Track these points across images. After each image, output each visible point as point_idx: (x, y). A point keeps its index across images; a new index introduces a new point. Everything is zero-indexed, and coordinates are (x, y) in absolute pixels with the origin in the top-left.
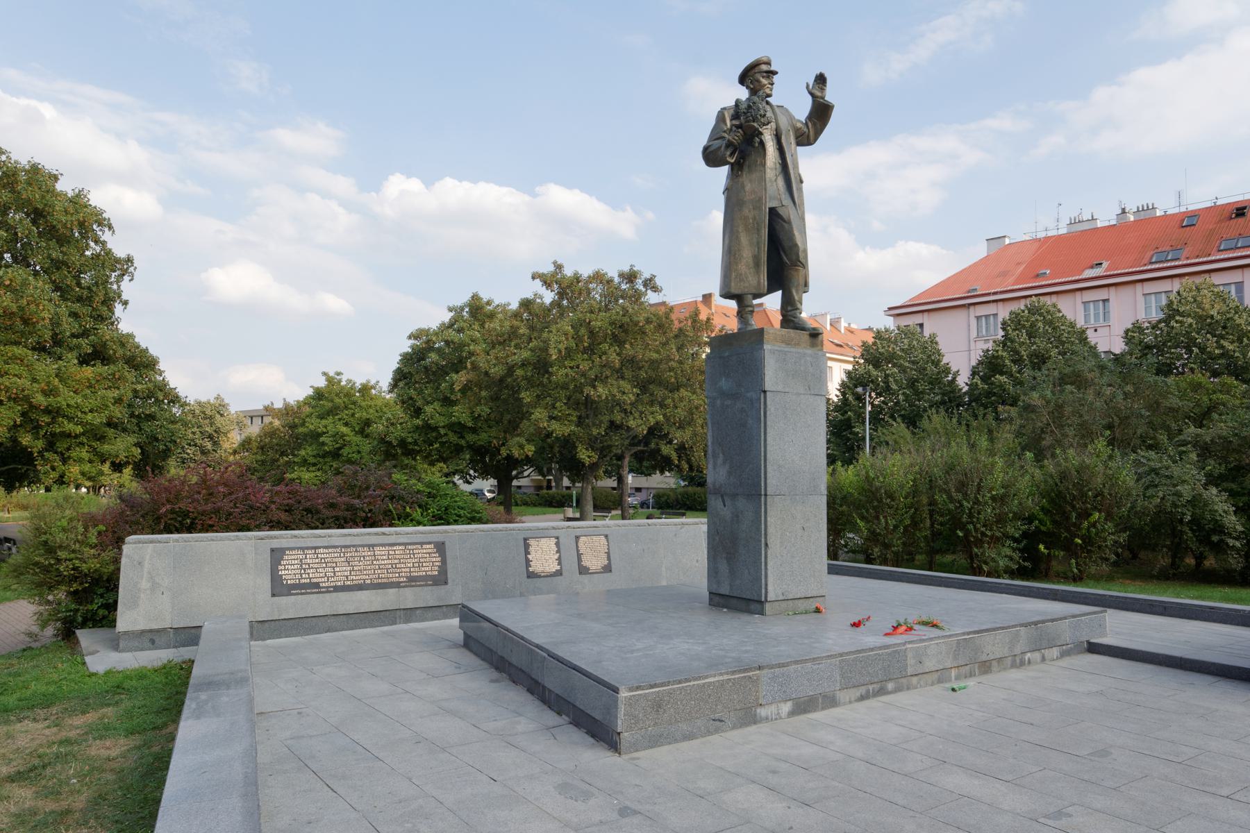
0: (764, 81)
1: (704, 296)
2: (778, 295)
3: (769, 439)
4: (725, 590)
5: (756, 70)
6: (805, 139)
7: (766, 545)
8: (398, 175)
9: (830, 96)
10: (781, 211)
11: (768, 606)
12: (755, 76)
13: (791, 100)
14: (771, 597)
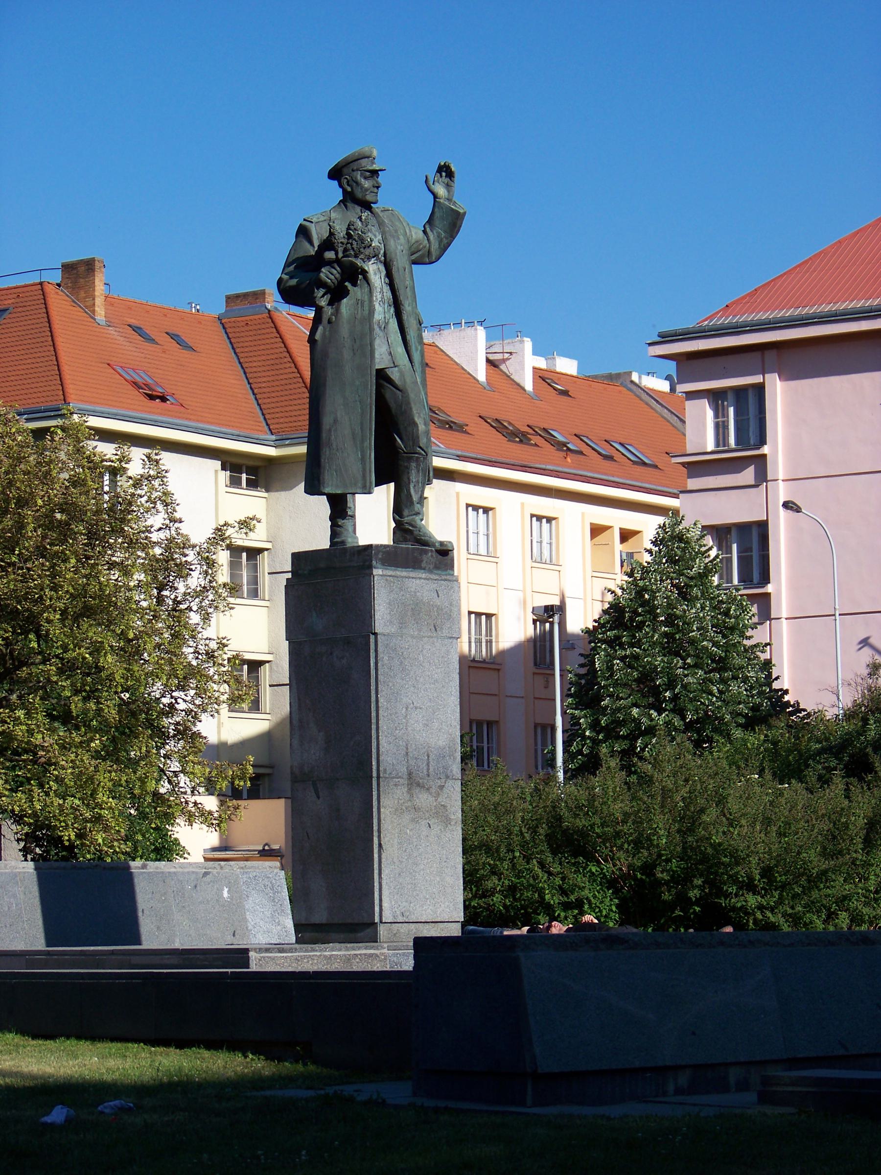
0: (367, 184)
1: (68, 268)
2: (385, 494)
3: (381, 700)
4: (320, 916)
5: (354, 166)
6: (422, 257)
7: (380, 845)
8: (286, 709)
9: (462, 199)
10: (394, 374)
11: (382, 930)
12: (352, 180)
13: (404, 207)
14: (387, 916)
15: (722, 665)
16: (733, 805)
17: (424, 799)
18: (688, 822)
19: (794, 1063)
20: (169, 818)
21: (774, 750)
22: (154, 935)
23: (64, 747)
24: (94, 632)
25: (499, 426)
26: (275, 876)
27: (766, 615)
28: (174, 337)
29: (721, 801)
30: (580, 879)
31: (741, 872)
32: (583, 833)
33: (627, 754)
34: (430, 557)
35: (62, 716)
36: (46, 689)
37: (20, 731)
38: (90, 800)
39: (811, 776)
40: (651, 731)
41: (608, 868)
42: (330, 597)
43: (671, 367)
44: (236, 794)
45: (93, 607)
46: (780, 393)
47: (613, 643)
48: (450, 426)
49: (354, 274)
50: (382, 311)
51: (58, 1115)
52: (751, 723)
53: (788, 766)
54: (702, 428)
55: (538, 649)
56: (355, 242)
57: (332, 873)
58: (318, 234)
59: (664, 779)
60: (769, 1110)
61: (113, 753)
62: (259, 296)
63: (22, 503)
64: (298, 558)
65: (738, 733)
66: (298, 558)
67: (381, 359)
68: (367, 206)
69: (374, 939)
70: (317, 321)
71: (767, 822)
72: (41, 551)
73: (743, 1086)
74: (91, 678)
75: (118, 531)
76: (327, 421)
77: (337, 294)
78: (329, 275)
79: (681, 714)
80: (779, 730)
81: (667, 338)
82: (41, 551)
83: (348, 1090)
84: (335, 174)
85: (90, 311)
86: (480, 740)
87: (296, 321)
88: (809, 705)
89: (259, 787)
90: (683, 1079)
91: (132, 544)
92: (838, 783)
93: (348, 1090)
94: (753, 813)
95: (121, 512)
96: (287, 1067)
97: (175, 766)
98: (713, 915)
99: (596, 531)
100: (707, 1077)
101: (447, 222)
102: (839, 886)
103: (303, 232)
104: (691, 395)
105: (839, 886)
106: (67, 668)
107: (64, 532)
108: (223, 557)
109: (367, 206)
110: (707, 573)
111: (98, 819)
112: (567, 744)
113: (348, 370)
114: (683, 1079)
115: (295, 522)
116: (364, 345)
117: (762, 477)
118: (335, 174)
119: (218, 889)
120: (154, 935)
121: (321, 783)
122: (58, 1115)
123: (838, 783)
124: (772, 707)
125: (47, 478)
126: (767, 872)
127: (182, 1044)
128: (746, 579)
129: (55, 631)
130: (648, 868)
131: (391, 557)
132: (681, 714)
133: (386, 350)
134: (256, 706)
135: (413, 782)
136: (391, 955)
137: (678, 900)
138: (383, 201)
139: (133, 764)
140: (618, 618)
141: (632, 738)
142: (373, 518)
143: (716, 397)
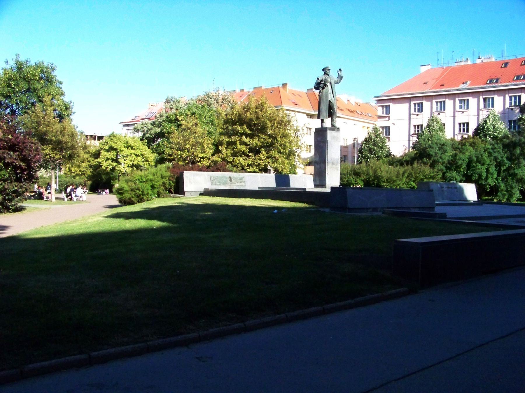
1: (283, 84)
4: (318, 184)
6: (336, 83)
9: (343, 74)
12: (326, 71)
13: (333, 75)
15: (382, 148)
16: (382, 169)
17: (334, 166)
18: (375, 172)
19: (388, 208)
20: (296, 168)
21: (389, 161)
22: (292, 186)
23: (280, 157)
24: (284, 139)
25: (349, 110)
26: (312, 177)
27: (389, 140)
28: (299, 95)
29: (380, 168)
30: (358, 180)
31: (383, 179)
32: (359, 173)
33: (367, 162)
34: (336, 129)
35: (280, 152)
36: (277, 148)
37: (273, 154)
38: (284, 165)
39: (395, 165)
40: (370, 158)
41: (363, 178)
42: (321, 135)
43: (376, 102)
44: (307, 165)
45: (284, 136)
46: (392, 106)
47: (365, 144)
48: (341, 110)
49: (325, 85)
50: (330, 91)
51: (276, 211)
52: (386, 157)
53: (391, 163)
54: (380, 111)
55: (354, 145)
56: (326, 80)
57: (320, 177)
58: (320, 79)
59: (371, 165)
60: (384, 215)
61: (288, 158)
62: (312, 89)
63: (274, 120)
64: (316, 129)
65: (384, 159)
66: (316, 129)
67: (329, 99)
68: (328, 75)
69: (326, 187)
70: (320, 92)
71: (387, 172)
72: (277, 127)
73: (380, 211)
74: (284, 146)
75: (289, 124)
76: (321, 108)
77: (323, 88)
78: (322, 85)
79: (375, 155)
80: (390, 158)
81: (375, 97)
82: (277, 127)
83: (320, 209)
84: (323, 70)
85: (286, 91)
86: (344, 158)
87: (317, 92)
88: (395, 155)
89: (310, 164)
90: (371, 210)
91: (291, 126)
92: (399, 167)
93: (320, 209)
94: (385, 170)
95: (289, 122)
96: (311, 206)
97: (297, 160)
98: (379, 186)
99: (363, 127)
100: (375, 210)
101: (340, 78)
102: (398, 182)
103: (318, 79)
104: (379, 106)
105: (398, 182)
106: (281, 145)
107: (281, 124)
108: (305, 129)
109: (328, 75)
110: (379, 134)
111: (285, 168)
112: (357, 159)
113: (324, 100)
114: (371, 210)
115: (316, 123)
116: (327, 96)
117: (389, 119)
118: (323, 70)
119: (303, 180)
120: (292, 186)
121: (319, 163)
122: (276, 211)
123: (399, 167)
124: (389, 155)
125: (278, 116)
126: (387, 180)
127: (295, 202)
128: (386, 135)
129: (279, 139)
130: (369, 178)
131: (331, 129)
132: (375, 155)
133: (330, 97)
134: (310, 152)
135: (333, 164)
136: (328, 190)
137: (373, 183)
138: (330, 74)
139: (291, 160)
140: (366, 141)
141: (367, 159)
142: (328, 123)
143: (383, 106)
